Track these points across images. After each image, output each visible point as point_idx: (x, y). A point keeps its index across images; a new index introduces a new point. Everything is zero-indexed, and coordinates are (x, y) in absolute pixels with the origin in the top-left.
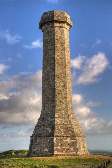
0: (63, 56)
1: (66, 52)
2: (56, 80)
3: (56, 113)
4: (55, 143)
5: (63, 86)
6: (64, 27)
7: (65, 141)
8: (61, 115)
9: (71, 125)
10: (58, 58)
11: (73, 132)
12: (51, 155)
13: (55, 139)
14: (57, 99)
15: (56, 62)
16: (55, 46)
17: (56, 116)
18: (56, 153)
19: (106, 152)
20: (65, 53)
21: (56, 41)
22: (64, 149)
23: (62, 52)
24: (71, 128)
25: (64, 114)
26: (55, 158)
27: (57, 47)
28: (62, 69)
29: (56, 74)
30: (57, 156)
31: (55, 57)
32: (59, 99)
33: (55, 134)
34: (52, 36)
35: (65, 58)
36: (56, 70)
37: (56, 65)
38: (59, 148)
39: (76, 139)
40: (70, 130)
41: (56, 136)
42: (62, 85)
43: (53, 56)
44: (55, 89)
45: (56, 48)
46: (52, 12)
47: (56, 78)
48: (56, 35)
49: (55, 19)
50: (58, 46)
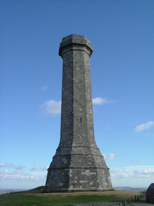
0: (83, 80)
3: (74, 141)
5: (82, 112)
8: (80, 144)
10: (77, 81)
15: (74, 85)
16: (74, 69)
17: (74, 145)
20: (84, 76)
21: (74, 64)
24: (91, 159)
25: (83, 142)
27: (75, 70)
29: (74, 98)
31: (73, 81)
32: (77, 126)
33: (71, 165)
34: (71, 59)
35: (85, 82)
36: (74, 93)
40: (90, 161)
41: (72, 168)
42: (81, 110)
45: (74, 71)
47: (74, 102)
48: (75, 58)
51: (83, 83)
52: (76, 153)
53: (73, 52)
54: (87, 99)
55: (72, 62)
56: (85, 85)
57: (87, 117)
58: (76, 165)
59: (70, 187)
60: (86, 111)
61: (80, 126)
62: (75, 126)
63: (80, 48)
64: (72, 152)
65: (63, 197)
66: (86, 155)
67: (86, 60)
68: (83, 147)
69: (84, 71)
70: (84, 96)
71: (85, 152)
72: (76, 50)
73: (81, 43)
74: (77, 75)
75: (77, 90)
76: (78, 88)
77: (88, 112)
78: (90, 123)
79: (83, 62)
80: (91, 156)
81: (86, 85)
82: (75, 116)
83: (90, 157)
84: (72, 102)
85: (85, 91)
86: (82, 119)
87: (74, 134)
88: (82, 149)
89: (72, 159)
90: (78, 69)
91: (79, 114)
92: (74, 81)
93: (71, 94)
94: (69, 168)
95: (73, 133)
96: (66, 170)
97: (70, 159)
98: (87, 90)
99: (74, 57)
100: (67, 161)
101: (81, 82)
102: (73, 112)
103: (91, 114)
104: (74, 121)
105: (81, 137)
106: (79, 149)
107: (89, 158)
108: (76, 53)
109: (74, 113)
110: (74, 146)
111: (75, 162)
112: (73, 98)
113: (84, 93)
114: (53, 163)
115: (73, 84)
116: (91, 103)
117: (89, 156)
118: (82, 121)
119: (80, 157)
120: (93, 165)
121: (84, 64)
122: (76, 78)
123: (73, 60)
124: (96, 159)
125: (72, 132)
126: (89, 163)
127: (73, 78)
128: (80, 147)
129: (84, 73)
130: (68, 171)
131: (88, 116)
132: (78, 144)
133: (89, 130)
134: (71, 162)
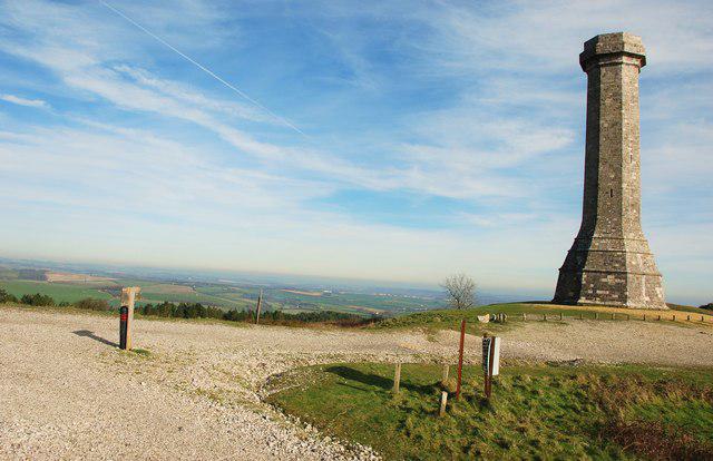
2: (601, 169)
3: (597, 229)
4: (584, 282)
6: (622, 63)
7: (604, 280)
10: (606, 125)
11: (624, 265)
12: (575, 304)
13: (584, 275)
14: (600, 204)
15: (602, 133)
17: (595, 235)
18: (582, 300)
22: (598, 296)
30: (581, 305)
32: (605, 204)
37: (602, 139)
38: (590, 292)
39: (626, 278)
41: (586, 271)
44: (597, 185)
45: (602, 107)
46: (621, 35)
49: (627, 49)
60: (621, 178)
72: (605, 65)
76: (607, 137)
79: (620, 87)
90: (608, 101)
106: (602, 242)
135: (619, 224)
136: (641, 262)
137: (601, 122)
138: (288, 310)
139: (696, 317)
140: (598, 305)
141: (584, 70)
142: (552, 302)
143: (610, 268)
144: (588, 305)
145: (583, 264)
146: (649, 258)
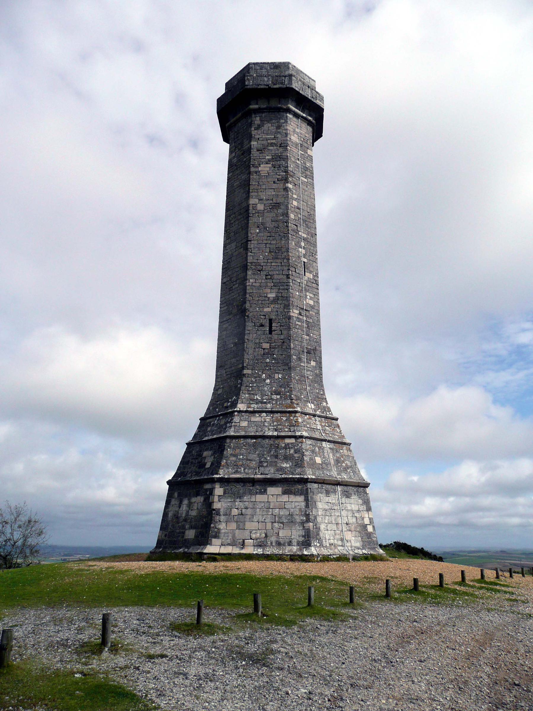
0: (280, 200)
1: (290, 186)
3: (244, 396)
5: (275, 300)
8: (262, 403)
9: (295, 437)
10: (260, 207)
12: (201, 557)
15: (253, 220)
16: (253, 169)
17: (241, 406)
19: (118, 553)
20: (286, 189)
21: (254, 153)
23: (275, 186)
24: (292, 451)
25: (274, 397)
26: (210, 567)
27: (256, 172)
28: (274, 242)
29: (250, 259)
30: (213, 558)
31: (248, 206)
32: (259, 345)
33: (221, 471)
34: (246, 142)
35: (287, 207)
36: (251, 245)
37: (254, 231)
40: (286, 458)
41: (223, 481)
42: (272, 295)
43: (244, 205)
45: (254, 177)
47: (249, 273)
48: (257, 137)
50: (260, 169)
51: (280, 211)
52: (243, 433)
53: (254, 119)
54: (292, 260)
55: (249, 150)
56: (287, 215)
57: (290, 318)
58: (240, 473)
59: (211, 544)
60: (287, 299)
61: (266, 346)
62: (249, 346)
63: (274, 103)
64: (233, 429)
65: (205, 574)
66: (278, 437)
67: (294, 138)
68: (272, 412)
69: (286, 172)
70: (283, 250)
71: (276, 430)
72: (259, 111)
73: (275, 87)
74: (264, 187)
75: (260, 234)
76: (262, 226)
77: (295, 301)
78: (305, 337)
79: (284, 146)
80: (293, 441)
81: (292, 216)
82: (251, 315)
83: (288, 444)
84: (244, 274)
85: (286, 236)
86: (273, 325)
87: (245, 372)
88: (268, 419)
89: (229, 451)
90: (264, 168)
91: (266, 310)
92: (251, 208)
93: (242, 250)
94: (213, 481)
95: (243, 368)
96: (208, 486)
97: (223, 451)
98: (297, 232)
99: (254, 132)
100: (215, 457)
101: (277, 206)
102: (245, 303)
103: (312, 307)
104: (247, 332)
105: (268, 381)
106: (256, 418)
107: (287, 447)
108: (261, 120)
109: (247, 305)
110: (240, 412)
111: (235, 462)
112: (247, 260)
113: (283, 242)
114: (182, 466)
115: (248, 217)
116: (311, 272)
117: (287, 441)
118: (273, 328)
119: (254, 445)
120: (298, 470)
121: (287, 150)
122: (257, 197)
123: (252, 143)
124: (313, 451)
125: (241, 366)
126: (285, 465)
127: (248, 198)
128: (263, 412)
129: (286, 181)
130: (211, 491)
131: (294, 313)
132: (257, 402)
133: (300, 359)
134: (224, 462)
135: (286, 384)
136: (331, 458)
137: (252, 201)
138: (239, 486)
139: (505, 558)
140: (249, 557)
141: (226, 139)
142: (153, 556)
143: (271, 473)
144: (229, 557)
145: (216, 466)
146: (344, 451)
